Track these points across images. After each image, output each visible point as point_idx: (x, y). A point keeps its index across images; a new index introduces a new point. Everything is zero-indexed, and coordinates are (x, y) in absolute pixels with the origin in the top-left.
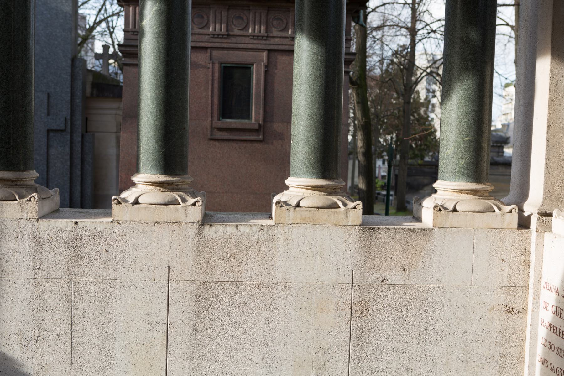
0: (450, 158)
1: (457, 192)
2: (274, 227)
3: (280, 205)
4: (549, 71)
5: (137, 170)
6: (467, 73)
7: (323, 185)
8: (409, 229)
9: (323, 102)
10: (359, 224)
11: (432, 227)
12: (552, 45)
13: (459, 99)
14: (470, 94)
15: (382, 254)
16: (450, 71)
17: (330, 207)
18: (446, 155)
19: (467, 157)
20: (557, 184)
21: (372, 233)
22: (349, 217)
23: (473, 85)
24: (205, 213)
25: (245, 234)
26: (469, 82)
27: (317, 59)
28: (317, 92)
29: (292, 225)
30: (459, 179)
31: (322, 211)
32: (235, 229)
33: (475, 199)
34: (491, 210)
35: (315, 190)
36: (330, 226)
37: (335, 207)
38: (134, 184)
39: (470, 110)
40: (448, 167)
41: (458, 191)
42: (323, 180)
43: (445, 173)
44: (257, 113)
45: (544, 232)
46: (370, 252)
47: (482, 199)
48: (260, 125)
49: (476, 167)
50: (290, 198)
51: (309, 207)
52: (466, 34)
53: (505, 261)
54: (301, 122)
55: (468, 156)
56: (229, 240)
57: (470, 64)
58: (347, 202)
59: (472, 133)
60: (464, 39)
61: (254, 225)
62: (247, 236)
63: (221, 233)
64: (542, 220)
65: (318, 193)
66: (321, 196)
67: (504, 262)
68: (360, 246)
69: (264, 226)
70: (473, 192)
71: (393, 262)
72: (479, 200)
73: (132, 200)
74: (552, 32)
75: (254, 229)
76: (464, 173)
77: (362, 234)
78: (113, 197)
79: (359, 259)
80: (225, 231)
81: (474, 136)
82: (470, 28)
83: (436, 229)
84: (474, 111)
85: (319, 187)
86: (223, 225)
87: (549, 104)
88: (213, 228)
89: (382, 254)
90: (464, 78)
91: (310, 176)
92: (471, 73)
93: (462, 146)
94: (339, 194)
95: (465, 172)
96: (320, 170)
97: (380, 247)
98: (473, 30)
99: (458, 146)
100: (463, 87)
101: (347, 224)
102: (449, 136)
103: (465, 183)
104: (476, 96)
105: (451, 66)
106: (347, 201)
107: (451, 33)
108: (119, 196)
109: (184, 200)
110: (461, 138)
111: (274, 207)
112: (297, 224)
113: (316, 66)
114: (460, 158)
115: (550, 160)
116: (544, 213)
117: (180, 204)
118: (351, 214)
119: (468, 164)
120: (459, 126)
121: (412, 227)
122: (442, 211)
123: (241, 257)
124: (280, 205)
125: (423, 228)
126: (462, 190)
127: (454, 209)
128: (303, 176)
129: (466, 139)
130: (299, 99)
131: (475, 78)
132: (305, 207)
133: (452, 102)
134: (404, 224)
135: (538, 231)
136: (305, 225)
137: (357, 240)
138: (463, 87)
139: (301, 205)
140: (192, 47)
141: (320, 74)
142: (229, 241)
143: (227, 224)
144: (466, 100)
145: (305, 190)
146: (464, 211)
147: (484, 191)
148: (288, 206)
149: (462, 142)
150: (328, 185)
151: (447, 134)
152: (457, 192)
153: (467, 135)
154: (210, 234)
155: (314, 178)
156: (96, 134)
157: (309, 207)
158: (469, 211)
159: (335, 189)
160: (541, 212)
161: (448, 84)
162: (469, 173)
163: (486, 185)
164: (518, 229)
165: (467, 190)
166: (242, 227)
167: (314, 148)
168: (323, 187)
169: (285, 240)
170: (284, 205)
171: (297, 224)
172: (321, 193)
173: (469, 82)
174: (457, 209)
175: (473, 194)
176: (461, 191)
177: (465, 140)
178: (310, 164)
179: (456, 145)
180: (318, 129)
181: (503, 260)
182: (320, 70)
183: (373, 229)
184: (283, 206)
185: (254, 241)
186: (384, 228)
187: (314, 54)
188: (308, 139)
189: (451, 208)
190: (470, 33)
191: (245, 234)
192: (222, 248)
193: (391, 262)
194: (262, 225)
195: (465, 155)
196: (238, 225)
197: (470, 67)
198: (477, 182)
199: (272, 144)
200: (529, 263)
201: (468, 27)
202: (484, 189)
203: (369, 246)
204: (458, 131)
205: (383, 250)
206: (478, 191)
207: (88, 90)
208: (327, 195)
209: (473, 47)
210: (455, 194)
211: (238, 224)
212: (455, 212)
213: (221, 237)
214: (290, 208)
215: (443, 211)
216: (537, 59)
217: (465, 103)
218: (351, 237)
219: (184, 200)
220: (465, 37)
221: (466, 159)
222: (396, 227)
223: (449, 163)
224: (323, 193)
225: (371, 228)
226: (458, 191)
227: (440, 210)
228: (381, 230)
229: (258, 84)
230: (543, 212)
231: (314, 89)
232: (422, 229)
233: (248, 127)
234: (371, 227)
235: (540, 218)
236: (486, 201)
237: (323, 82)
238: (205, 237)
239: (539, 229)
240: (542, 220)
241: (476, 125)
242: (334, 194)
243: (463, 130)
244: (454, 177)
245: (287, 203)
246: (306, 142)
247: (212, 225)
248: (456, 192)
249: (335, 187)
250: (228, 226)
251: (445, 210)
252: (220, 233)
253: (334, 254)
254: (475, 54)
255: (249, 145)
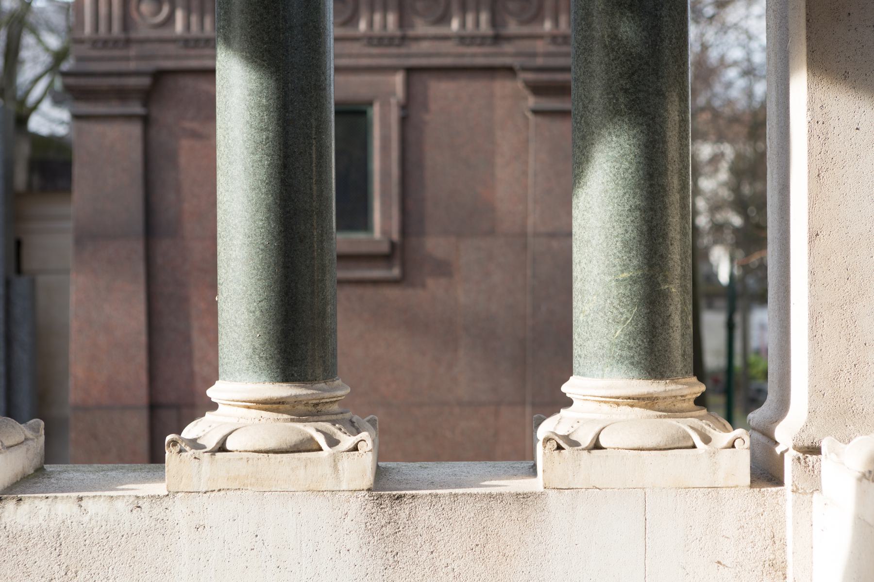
0: (590, 323)
1: (608, 402)
2: (167, 499)
3: (178, 448)
4: (806, 108)
5: (212, 379)
6: (616, 120)
7: (282, 398)
8: (485, 495)
9: (276, 203)
10: (366, 488)
11: (542, 489)
12: (808, 46)
13: (603, 183)
14: (627, 169)
15: (424, 557)
16: (582, 117)
17: (295, 449)
18: (582, 315)
19: (627, 319)
20: (842, 374)
21: (398, 508)
22: (341, 472)
23: (633, 148)
24: (378, 467)
25: (99, 519)
26: (622, 141)
27: (259, 106)
28: (262, 181)
29: (208, 494)
30: (611, 371)
31: (275, 458)
32: (75, 508)
33: (649, 417)
34: (685, 444)
35: (266, 410)
36: (297, 494)
37: (309, 448)
38: (568, 403)
39: (627, 207)
40: (586, 344)
41: (608, 399)
42: (285, 385)
43: (582, 358)
44: (385, 215)
45: (812, 492)
46: (394, 553)
47: (665, 417)
48: (393, 245)
49: (651, 342)
50: (207, 429)
51: (246, 451)
52: (610, 30)
53: (724, 565)
54: (231, 252)
55: (628, 315)
56: (62, 533)
57: (621, 100)
58: (340, 435)
59: (635, 262)
60: (607, 40)
61: (118, 497)
62: (104, 523)
63: (43, 518)
64: (806, 463)
65: (274, 415)
66: (278, 424)
67: (721, 567)
68: (371, 538)
69: (143, 498)
70: (647, 401)
71: (451, 575)
72: (659, 420)
73: (211, 442)
74: (807, 14)
75: (120, 505)
76: (621, 356)
77: (373, 511)
78: (169, 438)
79: (370, 570)
80: (53, 513)
81: (640, 268)
82: (618, 15)
83: (552, 493)
84: (637, 208)
85: (274, 403)
86: (47, 498)
87: (809, 186)
88: (25, 507)
89: (424, 557)
90: (610, 133)
91: (256, 376)
92: (626, 120)
93: (615, 293)
94: (324, 418)
95: (624, 353)
96: (278, 361)
97: (419, 541)
98: (625, 19)
99: (605, 293)
100: (610, 154)
101: (338, 489)
102: (586, 270)
103: (624, 380)
104: (641, 172)
105: (583, 104)
106: (712, 431)
107: (579, 28)
108: (180, 434)
109: (333, 442)
110: (610, 274)
111: (539, 447)
112: (220, 490)
113: (258, 121)
114: (610, 321)
115: (820, 320)
116: (808, 448)
117: (320, 449)
118: (348, 463)
119: (631, 336)
120: (605, 245)
121: (493, 491)
122: (563, 449)
123: (92, 572)
124: (178, 448)
125: (520, 491)
126: (618, 398)
127: (354, 448)
128: (239, 377)
129: (621, 276)
130: (225, 199)
131: (635, 131)
132: (237, 450)
133: (589, 190)
134: (483, 483)
135: (798, 489)
136: (239, 492)
137: (363, 526)
138: (610, 154)
139: (229, 446)
140: (337, 39)
141: (267, 138)
142: (61, 536)
143: (56, 497)
144: (617, 184)
145: (246, 410)
146: (618, 449)
147: (671, 397)
148: (197, 449)
149: (614, 283)
150: (296, 396)
151: (583, 265)
152: (608, 402)
153: (625, 267)
154: (18, 520)
155: (264, 382)
156: (41, 280)
157: (246, 451)
158: (630, 447)
159: (317, 404)
160: (801, 444)
161: (579, 148)
162: (633, 357)
163: (676, 383)
164: (751, 487)
165: (629, 398)
166: (91, 501)
167: (261, 311)
168: (283, 403)
169: (193, 530)
170: (188, 448)
171: (220, 490)
172: (280, 416)
173: (622, 141)
174: (603, 443)
175: (646, 407)
176: (618, 400)
177: (620, 278)
178: (254, 349)
179: (601, 291)
180: (269, 267)
181: (719, 562)
182: (267, 130)
183: (399, 497)
184: (186, 451)
185: (120, 535)
186: (426, 496)
187: (251, 93)
188: (247, 291)
189: (586, 440)
190: (620, 26)
191: (99, 519)
192: (47, 553)
193: (447, 574)
194: (138, 497)
195: (622, 314)
196: (82, 498)
197: (623, 106)
198: (656, 378)
199: (424, 286)
200: (785, 568)
201: (613, 14)
202: (669, 394)
203: (392, 538)
204: (603, 258)
205: (427, 547)
206: (657, 398)
207: (21, 178)
208: (292, 420)
209: (627, 60)
210: (605, 407)
211: (81, 494)
212: (596, 452)
213: (44, 528)
214: (201, 455)
215: (568, 450)
216: (791, 74)
217: (617, 190)
218: (348, 519)
219: (333, 442)
220: (609, 36)
221: (624, 323)
222: (454, 491)
223: (588, 335)
224: (286, 416)
225: (394, 496)
226: (608, 399)
227: (559, 448)
228: (420, 500)
229: (386, 140)
230: (806, 445)
231: (255, 174)
232: (518, 494)
233: (364, 249)
234: (394, 493)
235: (799, 458)
236: (673, 421)
237: (276, 157)
238: (8, 528)
239: (800, 487)
240: (806, 463)
241: (643, 242)
242: (311, 418)
243: (614, 254)
244: (600, 367)
245: (199, 441)
246: (243, 298)
247: (21, 500)
248: (605, 402)
249: (314, 402)
250: (58, 500)
251: (570, 446)
252: (41, 518)
253: (310, 560)
254: (633, 74)
255: (369, 292)
